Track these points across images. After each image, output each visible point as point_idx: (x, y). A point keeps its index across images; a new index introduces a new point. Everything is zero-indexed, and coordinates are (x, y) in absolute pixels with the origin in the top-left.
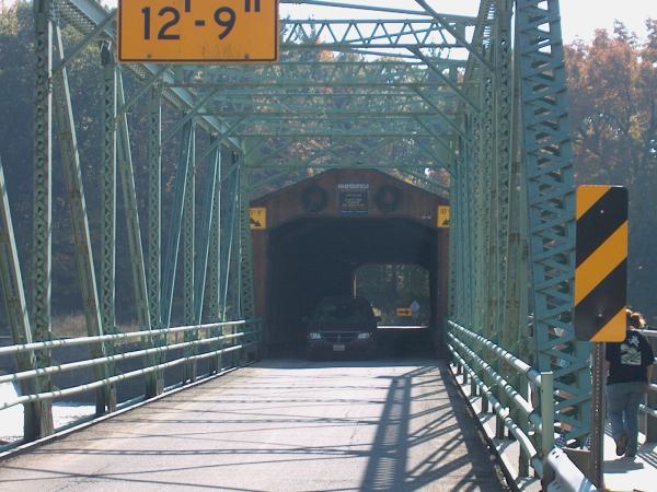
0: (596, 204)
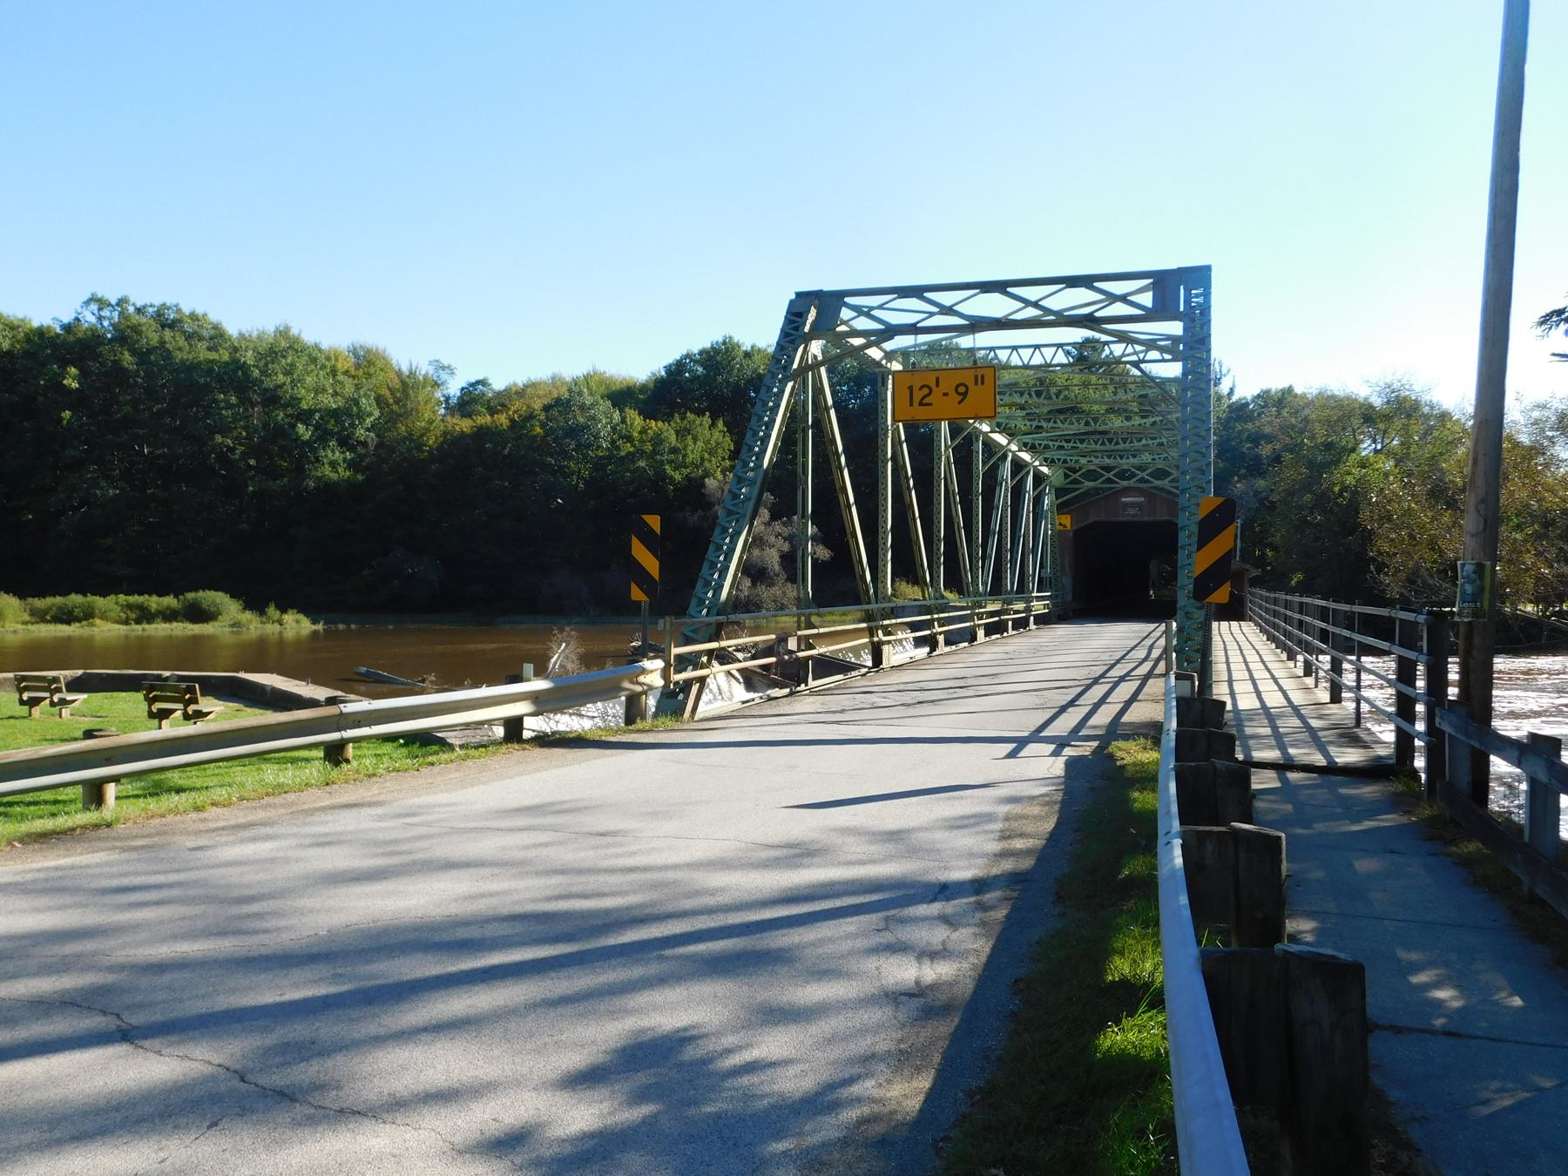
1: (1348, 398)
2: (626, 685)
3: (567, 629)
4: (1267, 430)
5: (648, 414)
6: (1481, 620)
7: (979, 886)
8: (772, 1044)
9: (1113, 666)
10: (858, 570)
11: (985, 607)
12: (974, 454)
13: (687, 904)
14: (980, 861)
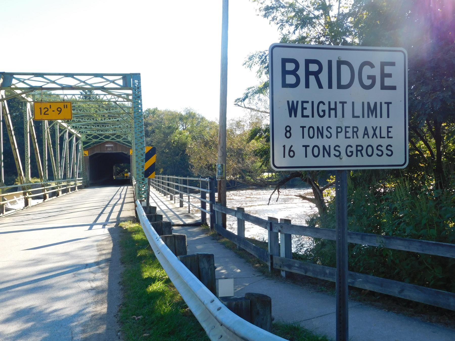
1: (175, 112)
4: (150, 122)
6: (223, 180)
7: (97, 263)
9: (110, 201)
10: (39, 172)
11: (61, 184)
12: (56, 130)
14: (94, 257)
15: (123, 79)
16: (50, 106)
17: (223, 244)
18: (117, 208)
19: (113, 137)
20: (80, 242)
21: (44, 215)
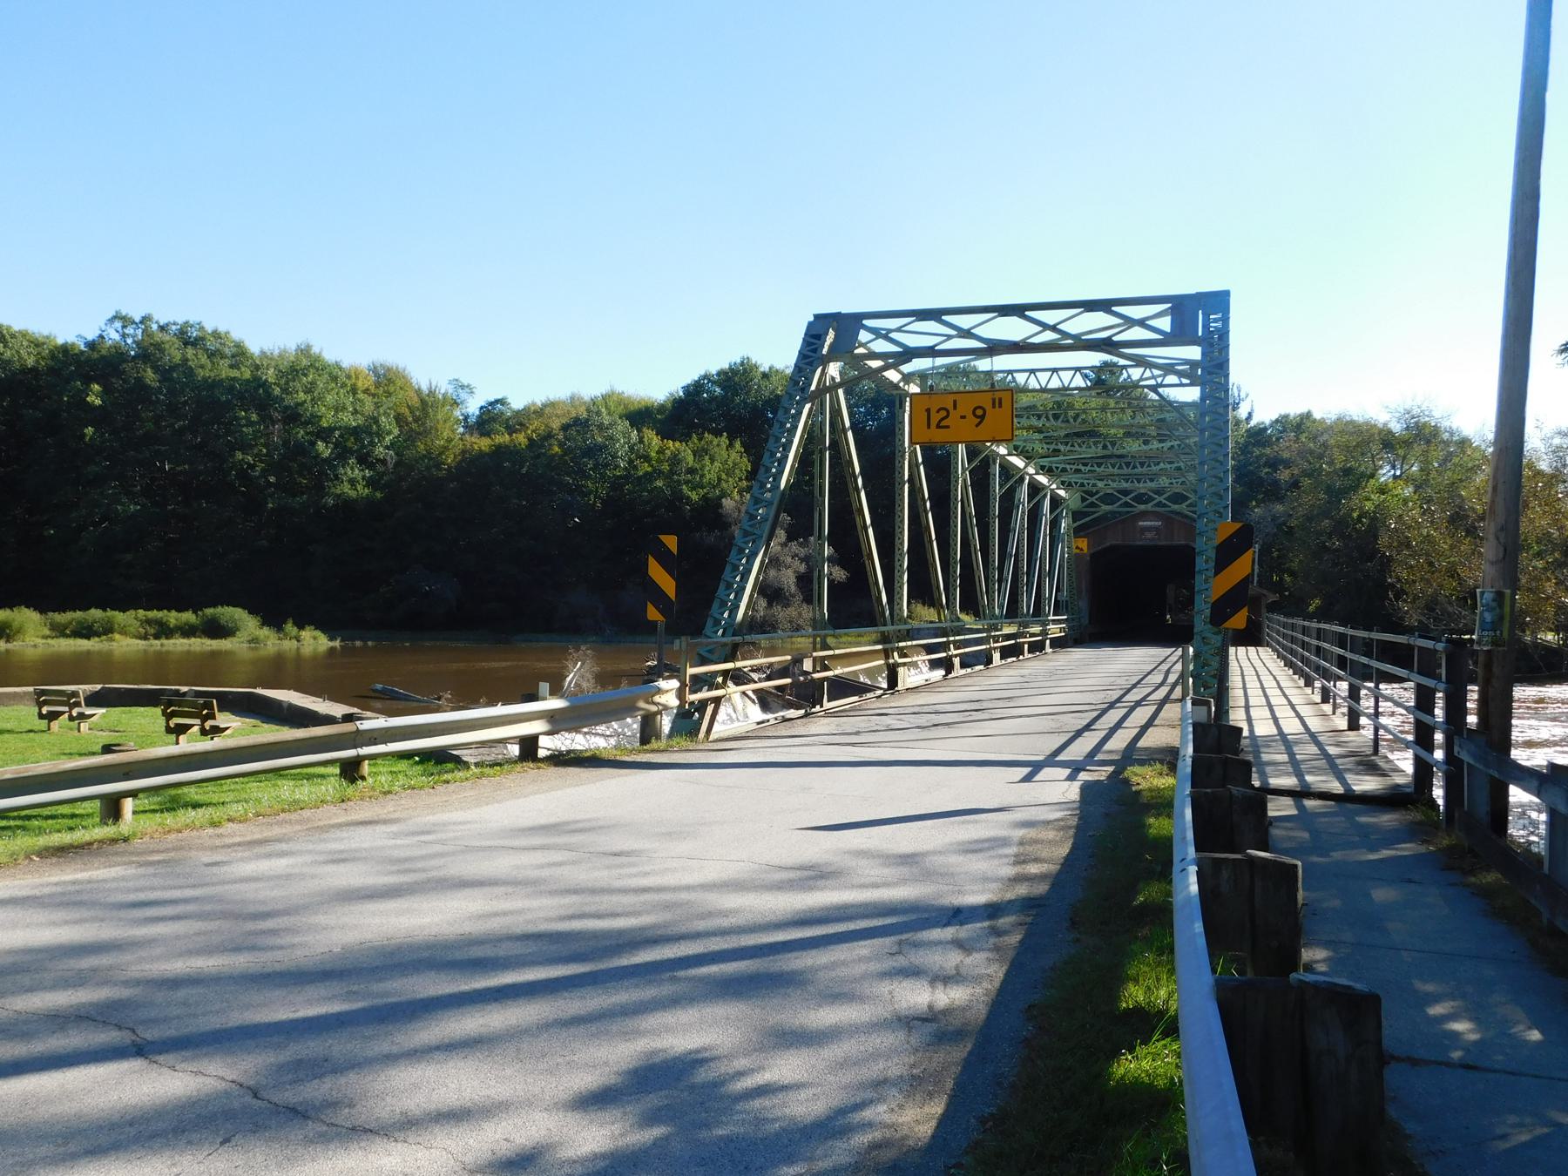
0: (1231, 535)
1: (1367, 423)
2: (642, 704)
3: (583, 648)
5: (665, 434)
7: (992, 911)
8: (785, 1067)
10: (874, 592)
11: (1001, 630)
12: (991, 476)
13: (701, 925)
14: (994, 886)
15: (1172, 315)
16: (955, 402)
17: (1485, 893)
18: (1142, 715)
19: (1127, 499)
20: (976, 822)
21: (923, 720)
